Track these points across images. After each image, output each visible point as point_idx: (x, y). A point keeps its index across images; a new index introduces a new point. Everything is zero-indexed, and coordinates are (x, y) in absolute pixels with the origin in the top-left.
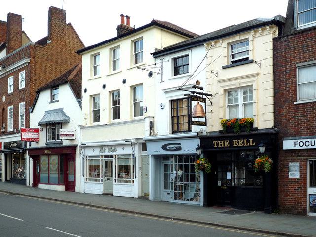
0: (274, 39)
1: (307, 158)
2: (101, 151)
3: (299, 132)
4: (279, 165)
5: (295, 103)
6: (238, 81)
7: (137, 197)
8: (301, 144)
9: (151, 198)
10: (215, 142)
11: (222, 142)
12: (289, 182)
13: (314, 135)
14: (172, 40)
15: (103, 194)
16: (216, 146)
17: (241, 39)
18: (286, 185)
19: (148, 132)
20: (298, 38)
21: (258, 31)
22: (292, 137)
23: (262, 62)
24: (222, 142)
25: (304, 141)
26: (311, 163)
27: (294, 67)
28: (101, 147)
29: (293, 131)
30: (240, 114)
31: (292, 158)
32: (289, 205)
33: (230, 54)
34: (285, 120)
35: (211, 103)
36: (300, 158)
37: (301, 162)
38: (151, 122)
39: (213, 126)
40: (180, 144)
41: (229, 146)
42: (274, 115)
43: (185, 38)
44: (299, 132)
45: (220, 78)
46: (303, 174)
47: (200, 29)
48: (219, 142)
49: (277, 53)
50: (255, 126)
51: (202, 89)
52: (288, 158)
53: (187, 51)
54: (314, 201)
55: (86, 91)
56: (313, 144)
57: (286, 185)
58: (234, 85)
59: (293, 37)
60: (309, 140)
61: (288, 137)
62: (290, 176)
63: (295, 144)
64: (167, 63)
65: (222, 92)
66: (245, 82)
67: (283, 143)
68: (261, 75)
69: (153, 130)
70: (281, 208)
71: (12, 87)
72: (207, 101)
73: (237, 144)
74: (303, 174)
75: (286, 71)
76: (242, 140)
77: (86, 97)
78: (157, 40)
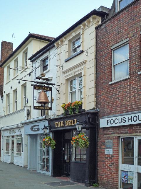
0: (97, 28)
1: (118, 135)
2: (10, 133)
3: (113, 111)
4: (99, 143)
5: (110, 83)
6: (72, 72)
7: (23, 166)
8: (112, 122)
9: (28, 169)
10: (56, 123)
11: (59, 122)
12: (106, 158)
13: (123, 113)
14: (43, 45)
15: (10, 163)
16: (56, 126)
17: (76, 34)
18: (104, 161)
19: (26, 118)
20: (112, 23)
21: (81, 27)
22: (108, 115)
23: (89, 51)
24: (59, 122)
25: (114, 118)
26: (123, 140)
27: (110, 50)
28: (10, 129)
29: (108, 110)
30: (77, 99)
31: (108, 136)
32: (105, 180)
33: (72, 49)
34: (103, 100)
35: (58, 91)
36: (113, 135)
37: (114, 139)
38: (28, 110)
39: (59, 110)
40: (38, 126)
41: (63, 126)
42: (96, 97)
43: (47, 43)
44: (113, 111)
45: (65, 69)
46: (116, 153)
47: (55, 35)
48: (58, 122)
49: (98, 41)
50: (83, 108)
51: (32, 85)
52: (105, 136)
53: (46, 54)
54: (125, 177)
55: (5, 92)
56: (120, 122)
57: (104, 161)
58: (71, 74)
59: (109, 23)
60: (118, 118)
61: (105, 116)
62: (106, 153)
63: (108, 122)
64: (38, 63)
65: (64, 81)
66: (77, 71)
67: (99, 121)
68: (88, 63)
69: (30, 116)
70: (100, 182)
71: (126, 66)
72: (53, 89)
73: (68, 124)
74: (115, 151)
75: (104, 55)
76: (70, 120)
77: (4, 95)
78: (34, 47)
